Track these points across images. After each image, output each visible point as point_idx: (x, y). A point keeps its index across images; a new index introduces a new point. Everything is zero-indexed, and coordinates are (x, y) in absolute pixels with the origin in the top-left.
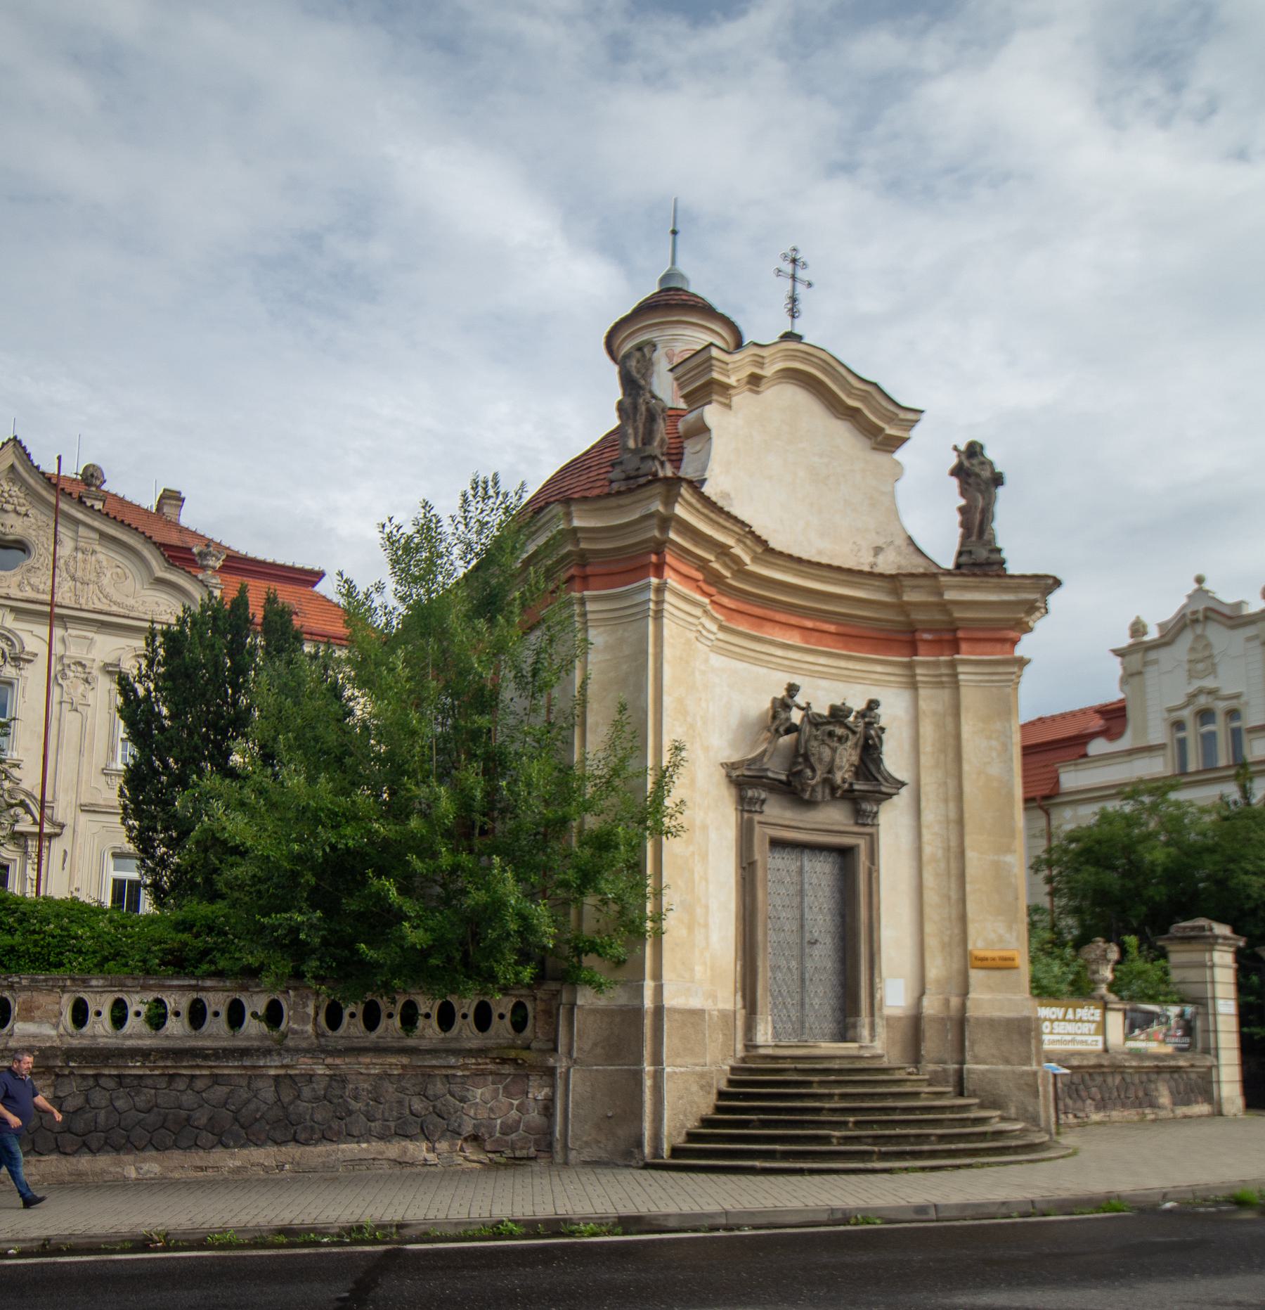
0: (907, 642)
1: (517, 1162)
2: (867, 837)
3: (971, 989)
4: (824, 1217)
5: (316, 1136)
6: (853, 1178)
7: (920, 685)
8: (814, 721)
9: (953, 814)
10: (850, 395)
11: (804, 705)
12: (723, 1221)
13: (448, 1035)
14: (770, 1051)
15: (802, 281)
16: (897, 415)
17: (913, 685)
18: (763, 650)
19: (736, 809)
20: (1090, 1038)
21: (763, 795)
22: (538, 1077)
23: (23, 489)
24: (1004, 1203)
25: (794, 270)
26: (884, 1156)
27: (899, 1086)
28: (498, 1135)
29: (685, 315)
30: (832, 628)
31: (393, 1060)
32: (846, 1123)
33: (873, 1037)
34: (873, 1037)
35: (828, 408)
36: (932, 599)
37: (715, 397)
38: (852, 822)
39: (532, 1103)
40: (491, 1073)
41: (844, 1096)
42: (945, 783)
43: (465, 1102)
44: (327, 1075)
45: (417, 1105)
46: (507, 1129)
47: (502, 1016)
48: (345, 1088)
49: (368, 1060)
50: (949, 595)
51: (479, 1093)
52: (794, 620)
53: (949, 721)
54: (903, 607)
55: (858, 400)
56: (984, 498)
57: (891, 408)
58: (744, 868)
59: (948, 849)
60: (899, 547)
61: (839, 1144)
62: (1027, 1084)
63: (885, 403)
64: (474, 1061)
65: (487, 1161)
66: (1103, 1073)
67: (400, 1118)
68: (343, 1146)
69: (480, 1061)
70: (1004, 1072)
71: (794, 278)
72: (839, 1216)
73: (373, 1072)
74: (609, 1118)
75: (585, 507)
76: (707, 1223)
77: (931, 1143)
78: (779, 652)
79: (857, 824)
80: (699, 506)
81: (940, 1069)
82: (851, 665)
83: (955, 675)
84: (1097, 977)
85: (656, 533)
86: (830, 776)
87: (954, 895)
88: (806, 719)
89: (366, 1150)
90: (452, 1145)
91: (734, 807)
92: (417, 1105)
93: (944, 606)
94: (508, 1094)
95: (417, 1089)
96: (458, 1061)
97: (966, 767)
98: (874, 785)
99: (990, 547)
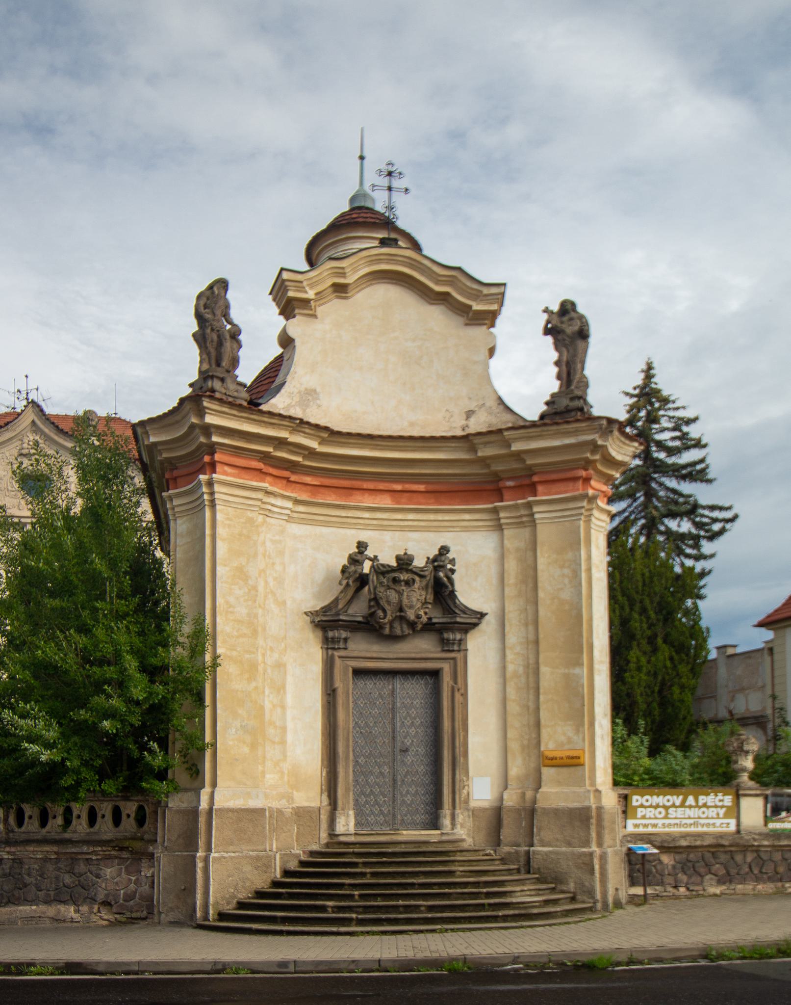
0: (494, 490)
1: (134, 921)
2: (452, 661)
3: (543, 784)
4: (208, 968)
5: (4, 901)
6: (311, 938)
7: (504, 527)
8: (381, 571)
9: (531, 637)
10: (438, 282)
11: (372, 556)
12: (136, 968)
13: (92, 830)
14: (352, 839)
15: (399, 190)
16: (481, 292)
17: (499, 528)
18: (349, 515)
19: (322, 648)
20: (718, 822)
21: (344, 634)
22: (148, 860)
23: (43, 437)
24: (353, 961)
25: (390, 182)
26: (361, 922)
27: (446, 866)
28: (121, 901)
29: (351, 232)
30: (422, 488)
31: (47, 848)
32: (353, 896)
33: (453, 825)
34: (453, 825)
35: (421, 297)
36: (503, 451)
37: (297, 311)
38: (439, 649)
39: (144, 879)
40: (116, 857)
41: (374, 875)
42: (526, 609)
43: (99, 878)
44: (11, 859)
45: (68, 879)
46: (129, 897)
47: (128, 816)
48: (22, 868)
49: (31, 849)
50: (516, 447)
51: (108, 872)
52: (381, 486)
53: (530, 554)
54: (484, 462)
55: (444, 285)
56: (568, 351)
57: (475, 286)
58: (329, 695)
59: (527, 666)
60: (490, 407)
61: (333, 912)
62: (583, 863)
63: (469, 283)
64: (100, 849)
65: (113, 920)
66: (731, 851)
67: (57, 889)
68: (21, 908)
69: (104, 848)
70: (564, 853)
71: (390, 189)
72: (220, 967)
73: (38, 857)
74: (184, 890)
75: (155, 426)
76: (125, 968)
77: (421, 912)
78: (367, 515)
79: (443, 651)
80: (235, 412)
81: (513, 851)
82: (440, 517)
83: (532, 515)
84: (736, 766)
85: (202, 439)
86: (403, 614)
87: (531, 705)
88: (373, 570)
89: (35, 911)
90: (91, 908)
91: (320, 646)
92: (68, 879)
93: (519, 456)
94: (128, 873)
95: (68, 869)
96: (89, 849)
97: (541, 594)
98: (451, 618)
99: (571, 396)
